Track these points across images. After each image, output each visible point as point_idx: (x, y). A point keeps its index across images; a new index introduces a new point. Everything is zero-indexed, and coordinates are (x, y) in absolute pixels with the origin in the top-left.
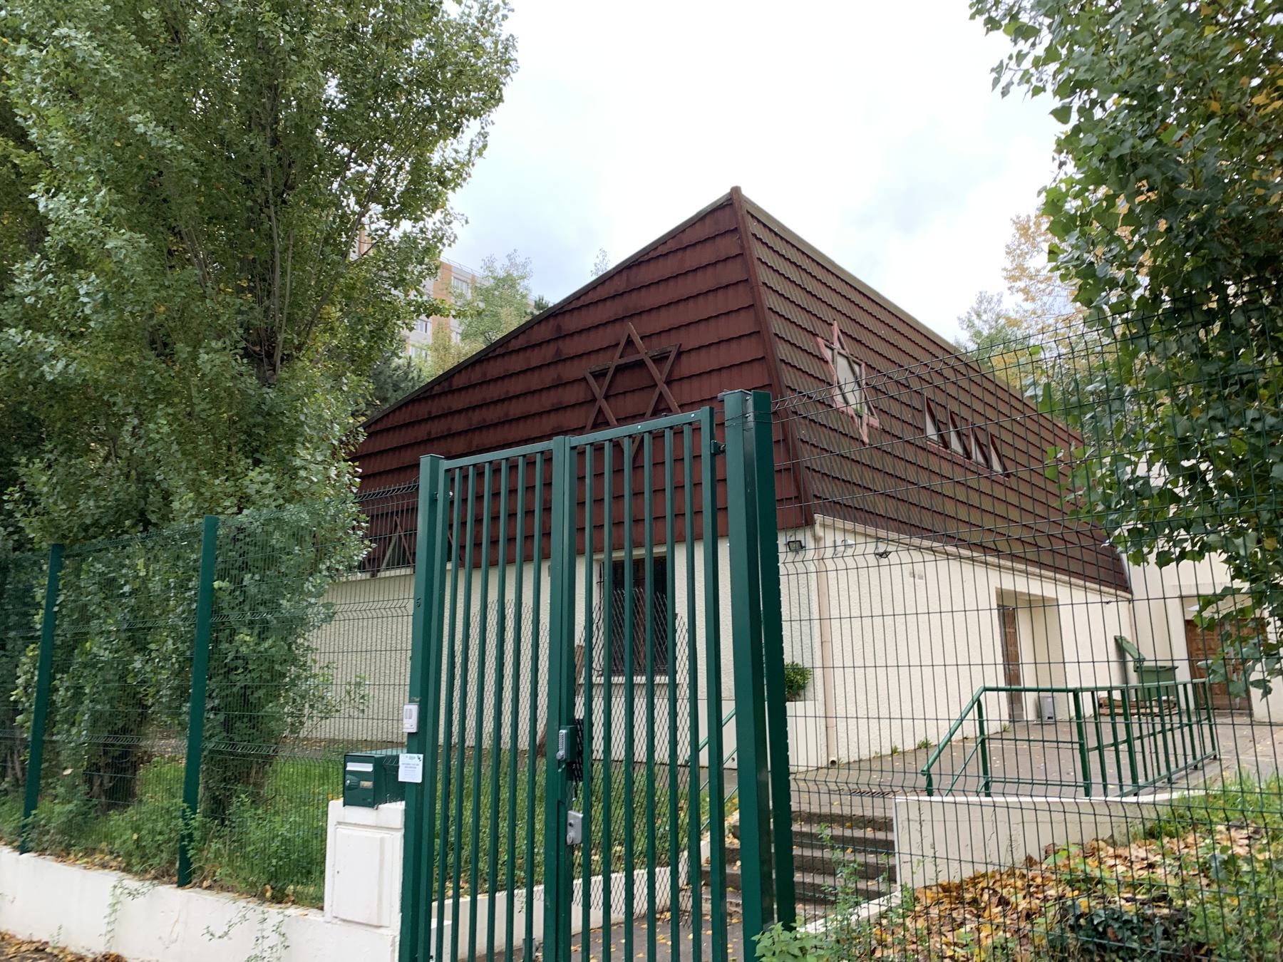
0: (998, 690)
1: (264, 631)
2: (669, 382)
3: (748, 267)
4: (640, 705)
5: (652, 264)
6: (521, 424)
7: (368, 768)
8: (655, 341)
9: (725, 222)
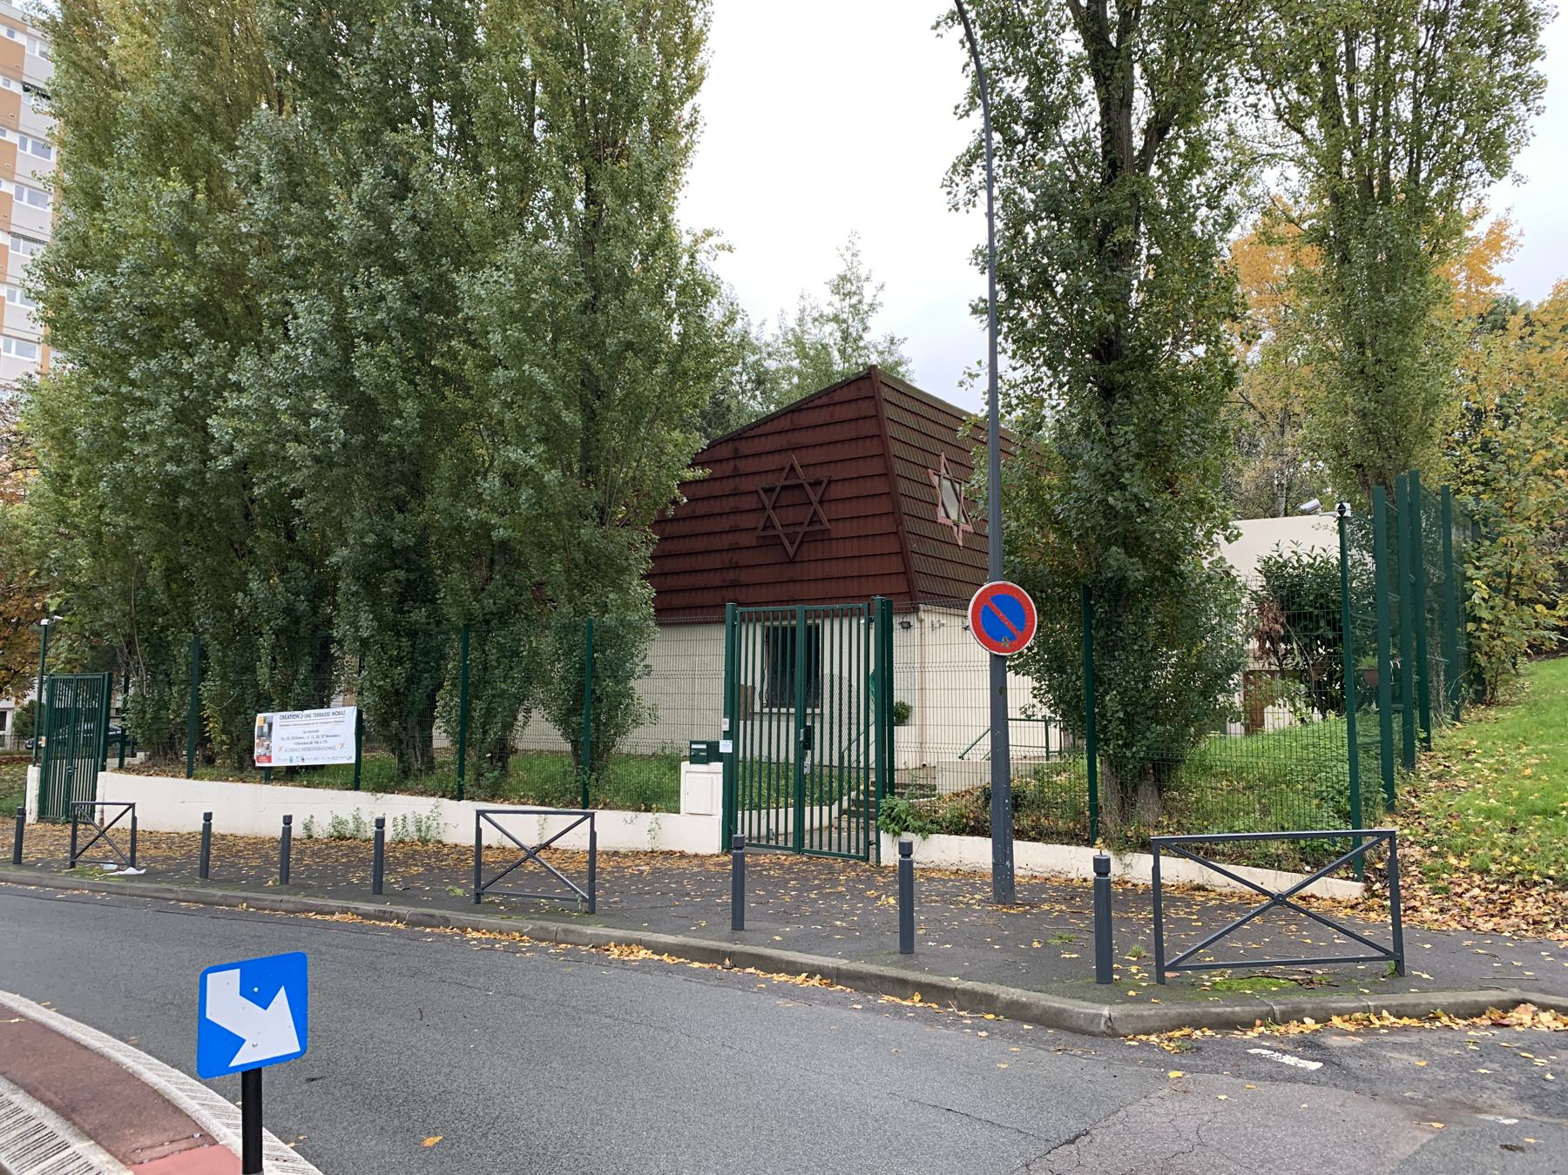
1: (617, 682)
2: (821, 502)
3: (881, 426)
4: (774, 724)
8: (811, 469)
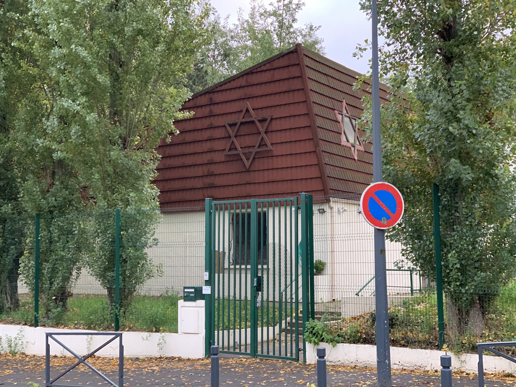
0: (389, 270)
5: (259, 74)
6: (192, 145)
7: (193, 290)
9: (293, 59)
